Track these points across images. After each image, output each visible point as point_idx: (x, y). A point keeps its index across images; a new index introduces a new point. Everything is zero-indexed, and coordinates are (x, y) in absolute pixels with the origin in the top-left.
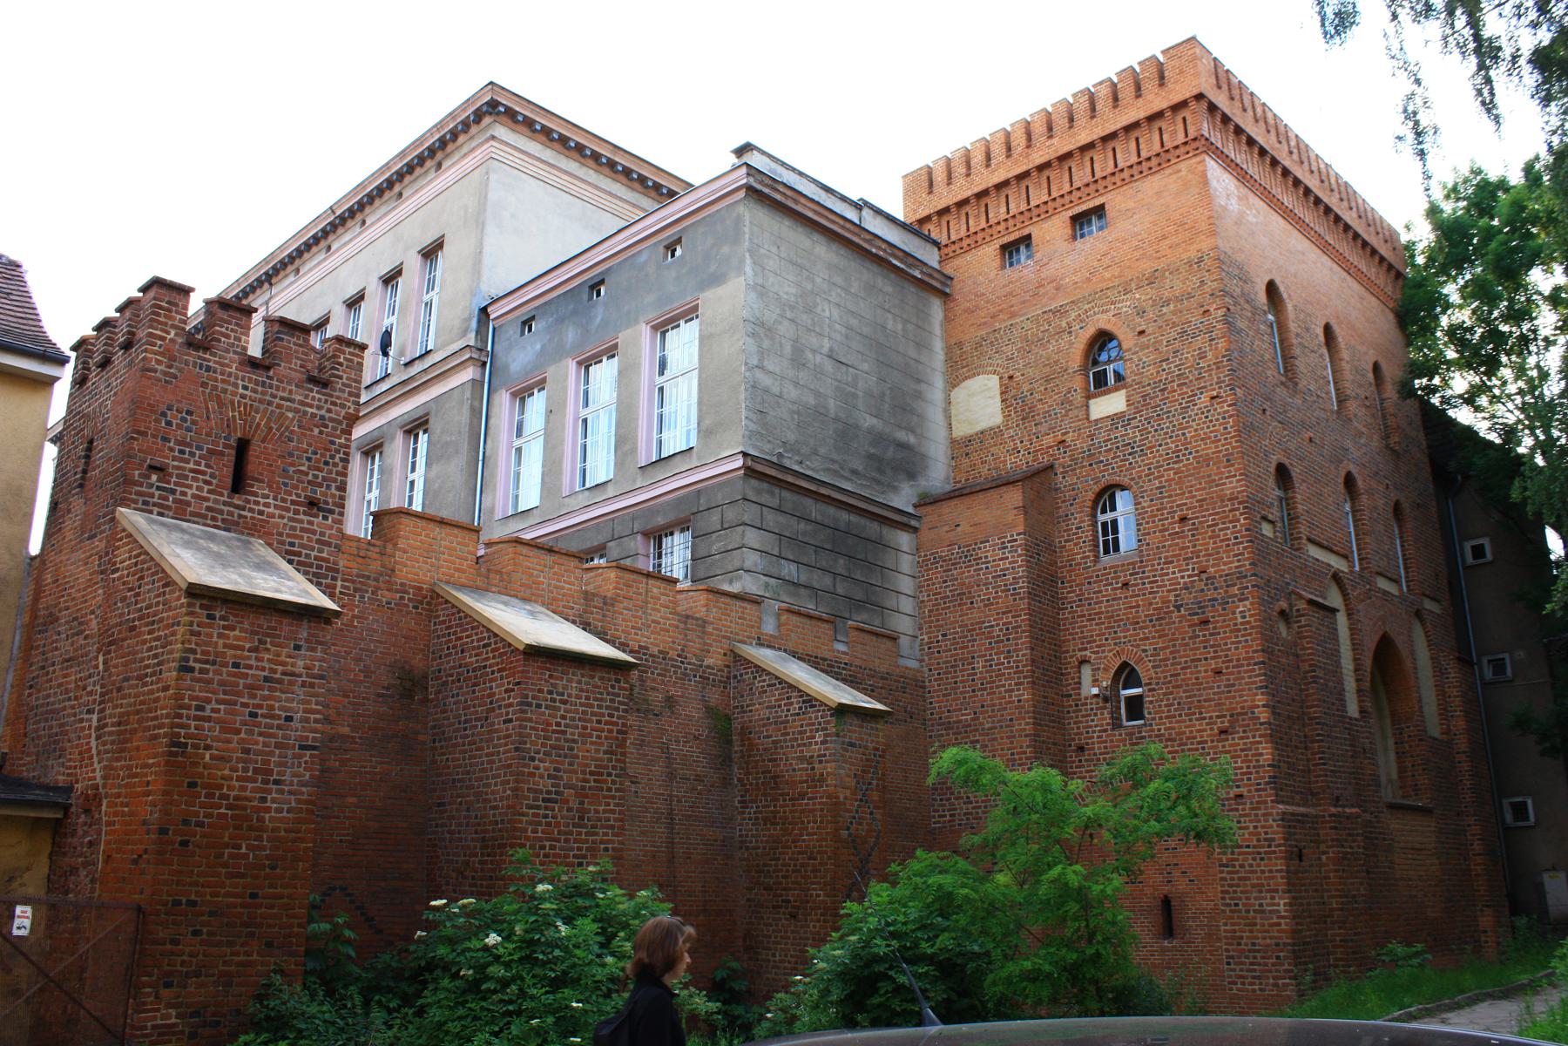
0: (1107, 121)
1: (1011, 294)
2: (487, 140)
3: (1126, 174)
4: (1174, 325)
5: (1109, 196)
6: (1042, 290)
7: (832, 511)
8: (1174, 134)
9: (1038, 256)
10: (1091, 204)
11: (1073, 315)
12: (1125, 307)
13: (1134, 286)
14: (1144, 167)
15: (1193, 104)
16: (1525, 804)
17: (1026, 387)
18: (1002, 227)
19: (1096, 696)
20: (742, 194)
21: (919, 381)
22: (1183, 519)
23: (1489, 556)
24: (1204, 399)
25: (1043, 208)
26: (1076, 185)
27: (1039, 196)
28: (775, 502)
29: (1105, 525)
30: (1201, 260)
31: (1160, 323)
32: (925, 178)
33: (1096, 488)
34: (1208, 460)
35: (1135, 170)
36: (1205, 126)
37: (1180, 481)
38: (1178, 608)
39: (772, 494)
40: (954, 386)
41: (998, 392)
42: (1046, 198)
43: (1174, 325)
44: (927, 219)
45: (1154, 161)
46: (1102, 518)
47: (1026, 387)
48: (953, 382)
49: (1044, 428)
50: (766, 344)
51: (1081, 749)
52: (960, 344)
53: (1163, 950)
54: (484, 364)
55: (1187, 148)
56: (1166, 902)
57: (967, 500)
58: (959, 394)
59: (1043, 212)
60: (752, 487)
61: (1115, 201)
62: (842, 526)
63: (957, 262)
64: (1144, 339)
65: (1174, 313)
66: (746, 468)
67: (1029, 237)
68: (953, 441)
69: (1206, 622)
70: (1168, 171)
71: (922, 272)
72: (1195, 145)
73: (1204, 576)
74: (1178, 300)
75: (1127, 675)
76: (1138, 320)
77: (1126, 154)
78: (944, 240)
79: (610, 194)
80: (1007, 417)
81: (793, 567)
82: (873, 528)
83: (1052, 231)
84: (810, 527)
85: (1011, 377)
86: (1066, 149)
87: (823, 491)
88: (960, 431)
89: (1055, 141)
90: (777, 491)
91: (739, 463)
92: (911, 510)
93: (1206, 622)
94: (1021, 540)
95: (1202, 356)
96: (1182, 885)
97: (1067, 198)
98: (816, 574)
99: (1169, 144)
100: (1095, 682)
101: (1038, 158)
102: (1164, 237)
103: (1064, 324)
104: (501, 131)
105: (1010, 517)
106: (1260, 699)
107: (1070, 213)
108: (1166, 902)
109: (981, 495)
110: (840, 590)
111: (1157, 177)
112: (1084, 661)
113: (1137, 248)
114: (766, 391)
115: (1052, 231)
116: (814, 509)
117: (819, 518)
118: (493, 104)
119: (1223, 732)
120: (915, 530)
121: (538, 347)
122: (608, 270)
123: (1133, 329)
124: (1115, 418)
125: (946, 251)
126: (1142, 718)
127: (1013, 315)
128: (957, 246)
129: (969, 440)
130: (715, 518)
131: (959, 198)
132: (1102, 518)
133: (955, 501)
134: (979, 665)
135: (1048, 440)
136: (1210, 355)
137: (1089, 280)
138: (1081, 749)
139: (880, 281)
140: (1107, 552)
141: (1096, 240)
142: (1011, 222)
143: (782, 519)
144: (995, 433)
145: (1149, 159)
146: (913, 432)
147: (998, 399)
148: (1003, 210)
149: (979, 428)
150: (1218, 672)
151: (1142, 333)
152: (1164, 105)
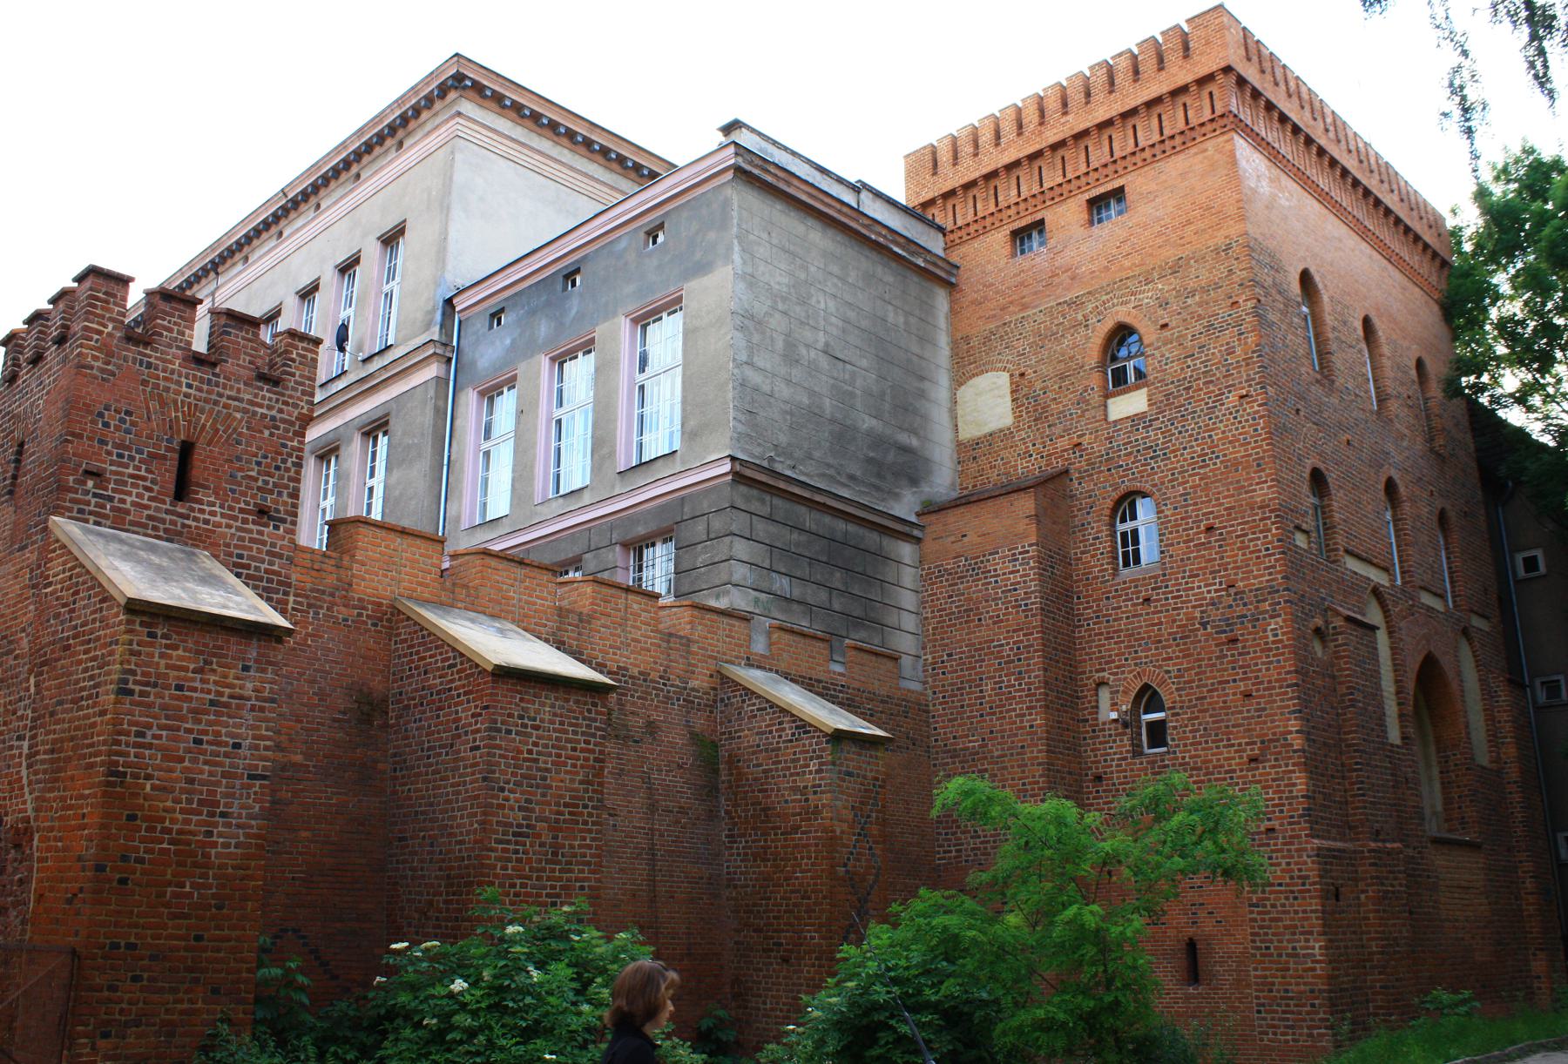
1: (1022, 284)
2: (452, 117)
4: (1200, 317)
5: (1129, 177)
6: (1056, 280)
7: (827, 519)
9: (1052, 243)
11: (1090, 307)
12: (1147, 298)
13: (1156, 275)
15: (1220, 78)
17: (1038, 385)
18: (1012, 211)
19: (1115, 721)
20: (729, 175)
21: (922, 378)
22: (1210, 529)
24: (1232, 398)
25: (1057, 191)
27: (1052, 178)
28: (765, 511)
30: (1229, 247)
32: (929, 157)
34: (1236, 464)
37: (1207, 488)
38: (1204, 625)
39: (763, 501)
40: (960, 384)
41: (1008, 391)
42: (1060, 180)
43: (1200, 317)
45: (1178, 140)
47: (1038, 385)
48: (959, 381)
49: (1058, 430)
50: (756, 338)
52: (967, 339)
53: (1188, 998)
54: (450, 360)
55: (1214, 125)
56: (1191, 945)
57: (974, 508)
58: (965, 393)
59: (1058, 195)
61: (1135, 183)
62: (839, 537)
63: (963, 249)
64: (1167, 333)
65: (1200, 305)
66: (733, 472)
67: (1041, 222)
68: (960, 446)
69: (1234, 641)
71: (925, 260)
73: (1232, 591)
74: (1205, 290)
75: (1148, 697)
76: (1160, 312)
77: (1148, 133)
78: (949, 226)
79: (586, 175)
80: (1018, 417)
81: (785, 581)
82: (872, 538)
83: (1067, 217)
84: (804, 538)
85: (1022, 375)
88: (968, 432)
89: (1070, 118)
90: (768, 498)
91: (727, 467)
92: (913, 519)
93: (1234, 641)
95: (1231, 352)
96: (1208, 927)
97: (1084, 180)
98: (811, 589)
99: (1194, 122)
101: (1052, 136)
102: (1189, 223)
103: (1080, 317)
104: (468, 107)
105: (1021, 527)
106: (1294, 725)
107: (1087, 196)
108: (1191, 945)
109: (990, 503)
110: (836, 606)
111: (1182, 156)
113: (1160, 234)
114: (756, 389)
115: (1067, 217)
116: (809, 518)
117: (814, 528)
118: (459, 78)
119: (1253, 760)
120: (918, 540)
121: (508, 341)
123: (1155, 322)
125: (951, 237)
126: (1165, 744)
127: (1025, 307)
128: (963, 233)
129: (976, 443)
131: (966, 179)
132: (1121, 528)
133: (962, 509)
134: (988, 687)
135: (1063, 443)
136: (1238, 351)
137: (1107, 269)
139: (879, 270)
140: (1126, 564)
141: (1115, 225)
142: (1022, 206)
143: (773, 528)
144: (1005, 435)
145: (1172, 137)
146: (916, 434)
147: (1008, 399)
148: (1014, 192)
149: (987, 429)
150: (1248, 695)
151: (1165, 326)
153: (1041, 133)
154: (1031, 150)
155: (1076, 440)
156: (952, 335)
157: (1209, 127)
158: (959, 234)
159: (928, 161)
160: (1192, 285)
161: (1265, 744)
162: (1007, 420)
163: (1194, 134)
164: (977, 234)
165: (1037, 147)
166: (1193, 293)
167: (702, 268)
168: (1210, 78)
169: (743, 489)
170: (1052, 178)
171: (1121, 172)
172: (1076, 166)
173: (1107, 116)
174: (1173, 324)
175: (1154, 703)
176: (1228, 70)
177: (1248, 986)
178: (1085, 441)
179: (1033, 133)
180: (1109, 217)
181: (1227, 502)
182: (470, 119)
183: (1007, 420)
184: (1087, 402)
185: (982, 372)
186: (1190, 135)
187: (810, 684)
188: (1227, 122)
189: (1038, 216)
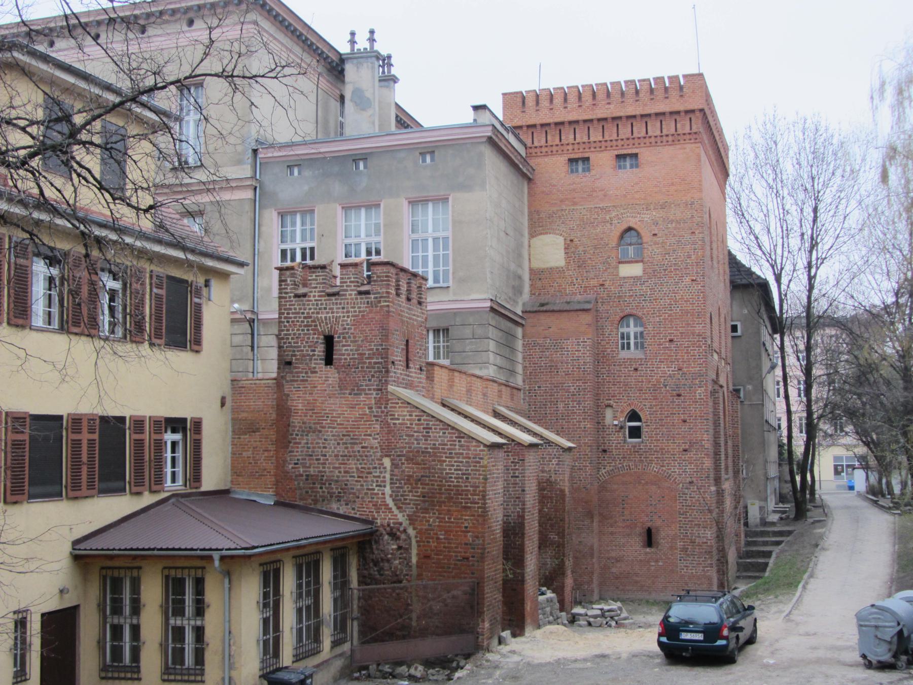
0: (645, 105)
1: (574, 190)
3: (653, 140)
4: (674, 235)
5: (642, 150)
6: (595, 194)
8: (684, 126)
9: (593, 173)
10: (630, 151)
11: (614, 214)
12: (647, 217)
13: (652, 207)
14: (663, 140)
15: (698, 114)
16: (630, 428)
17: (581, 249)
18: (570, 147)
20: (484, 140)
23: (739, 333)
24: (687, 279)
25: (598, 144)
26: (620, 137)
27: (596, 136)
29: (623, 334)
31: (666, 232)
33: (622, 315)
36: (698, 126)
37: (671, 321)
38: (665, 386)
40: (533, 237)
42: (600, 138)
43: (674, 235)
45: (670, 138)
46: (621, 330)
49: (592, 275)
52: (538, 212)
53: (646, 553)
54: (255, 188)
55: (691, 136)
59: (602, 146)
61: (645, 154)
63: (539, 160)
64: (655, 239)
65: (675, 228)
69: (679, 395)
70: (678, 147)
72: (695, 136)
74: (678, 222)
75: (634, 416)
77: (654, 129)
78: (529, 144)
80: (568, 263)
83: (603, 160)
85: (572, 241)
88: (536, 265)
89: (612, 106)
91: (488, 304)
92: (520, 314)
93: (679, 395)
94: (589, 342)
96: (659, 523)
97: (614, 143)
99: (680, 131)
100: (615, 418)
102: (673, 184)
103: (608, 218)
107: (616, 153)
109: (565, 314)
111: (671, 148)
112: (609, 406)
113: (656, 186)
115: (603, 160)
119: (685, 450)
120: (523, 325)
121: (306, 188)
122: (371, 153)
123: (650, 231)
125: (531, 151)
126: (639, 437)
127: (575, 204)
128: (538, 150)
130: (468, 332)
131: (544, 121)
132: (621, 330)
134: (561, 406)
136: (693, 257)
137: (625, 196)
140: (623, 348)
142: (576, 146)
144: (559, 271)
145: (667, 136)
147: (563, 251)
148: (572, 137)
150: (685, 421)
151: (655, 235)
153: (593, 110)
154: (586, 117)
155: (601, 282)
157: (688, 137)
158: (536, 150)
159: (516, 101)
160: (671, 217)
163: (679, 138)
165: (590, 117)
166: (672, 222)
167: (464, 187)
168: (693, 111)
171: (636, 145)
172: (611, 133)
173: (633, 113)
174: (659, 235)
176: (702, 110)
177: (676, 549)
178: (607, 284)
179: (588, 108)
180: (625, 168)
183: (562, 263)
185: (546, 233)
186: (676, 138)
187: (507, 407)
188: (693, 136)
189: (586, 155)
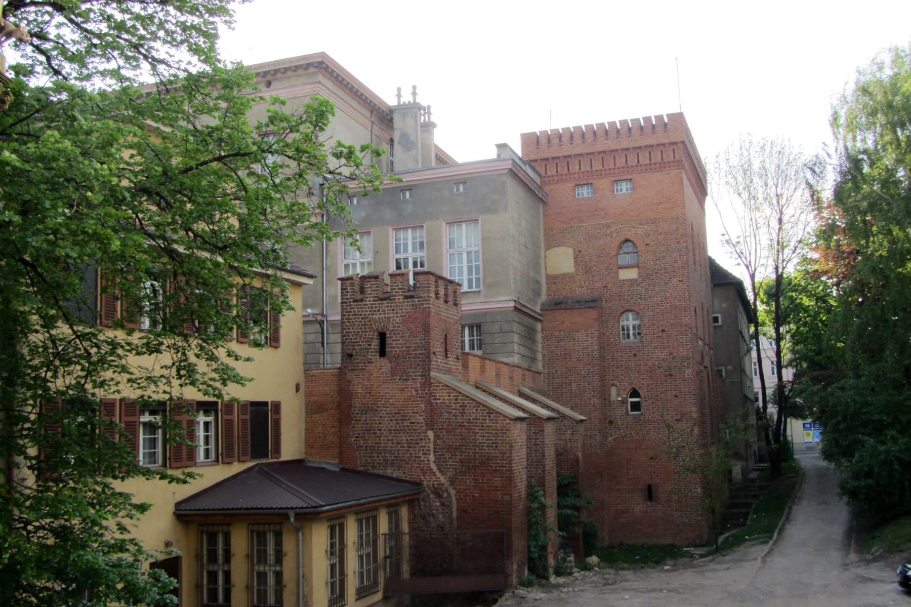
2: (316, 83)
4: (663, 245)
11: (613, 229)
20: (506, 171)
22: (663, 331)
23: (720, 323)
30: (677, 218)
32: (535, 142)
34: (676, 307)
35: (648, 167)
37: (663, 314)
38: (660, 368)
42: (601, 168)
43: (663, 245)
44: (536, 161)
45: (658, 166)
47: (587, 258)
48: (548, 248)
51: (611, 422)
56: (649, 487)
58: (548, 252)
60: (516, 317)
64: (648, 248)
66: (515, 307)
69: (671, 375)
79: (342, 99)
80: (577, 270)
85: (580, 251)
86: (615, 148)
87: (524, 310)
88: (551, 272)
89: (609, 142)
91: (512, 304)
95: (676, 262)
97: (612, 171)
100: (619, 395)
102: (661, 203)
104: (320, 78)
106: (694, 409)
108: (649, 487)
118: (321, 63)
119: (677, 420)
120: (541, 321)
121: (364, 214)
124: (633, 281)
126: (639, 410)
127: (581, 221)
128: (551, 179)
129: (556, 277)
134: (574, 386)
135: (598, 285)
137: (622, 214)
138: (611, 422)
147: (572, 261)
150: (676, 396)
151: (647, 245)
152: (666, 141)
154: (589, 151)
156: (544, 226)
161: (683, 415)
162: (572, 269)
164: (558, 182)
166: (661, 234)
169: (516, 313)
170: (597, 166)
175: (638, 395)
181: (671, 322)
182: (323, 85)
183: (572, 269)
184: (611, 270)
